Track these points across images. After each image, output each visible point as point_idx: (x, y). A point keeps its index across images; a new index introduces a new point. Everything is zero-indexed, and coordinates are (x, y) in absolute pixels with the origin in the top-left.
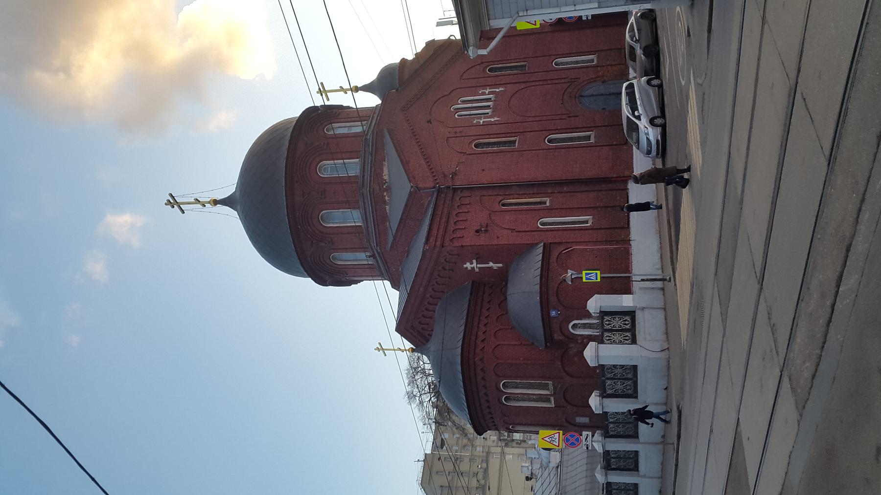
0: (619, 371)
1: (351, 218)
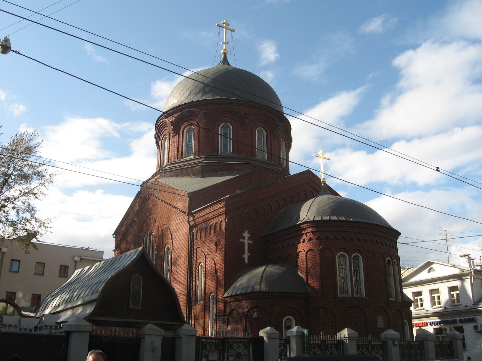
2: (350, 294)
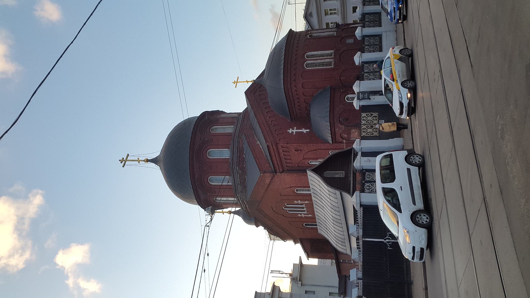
0: (372, 49)
1: (224, 154)
2: (331, 60)
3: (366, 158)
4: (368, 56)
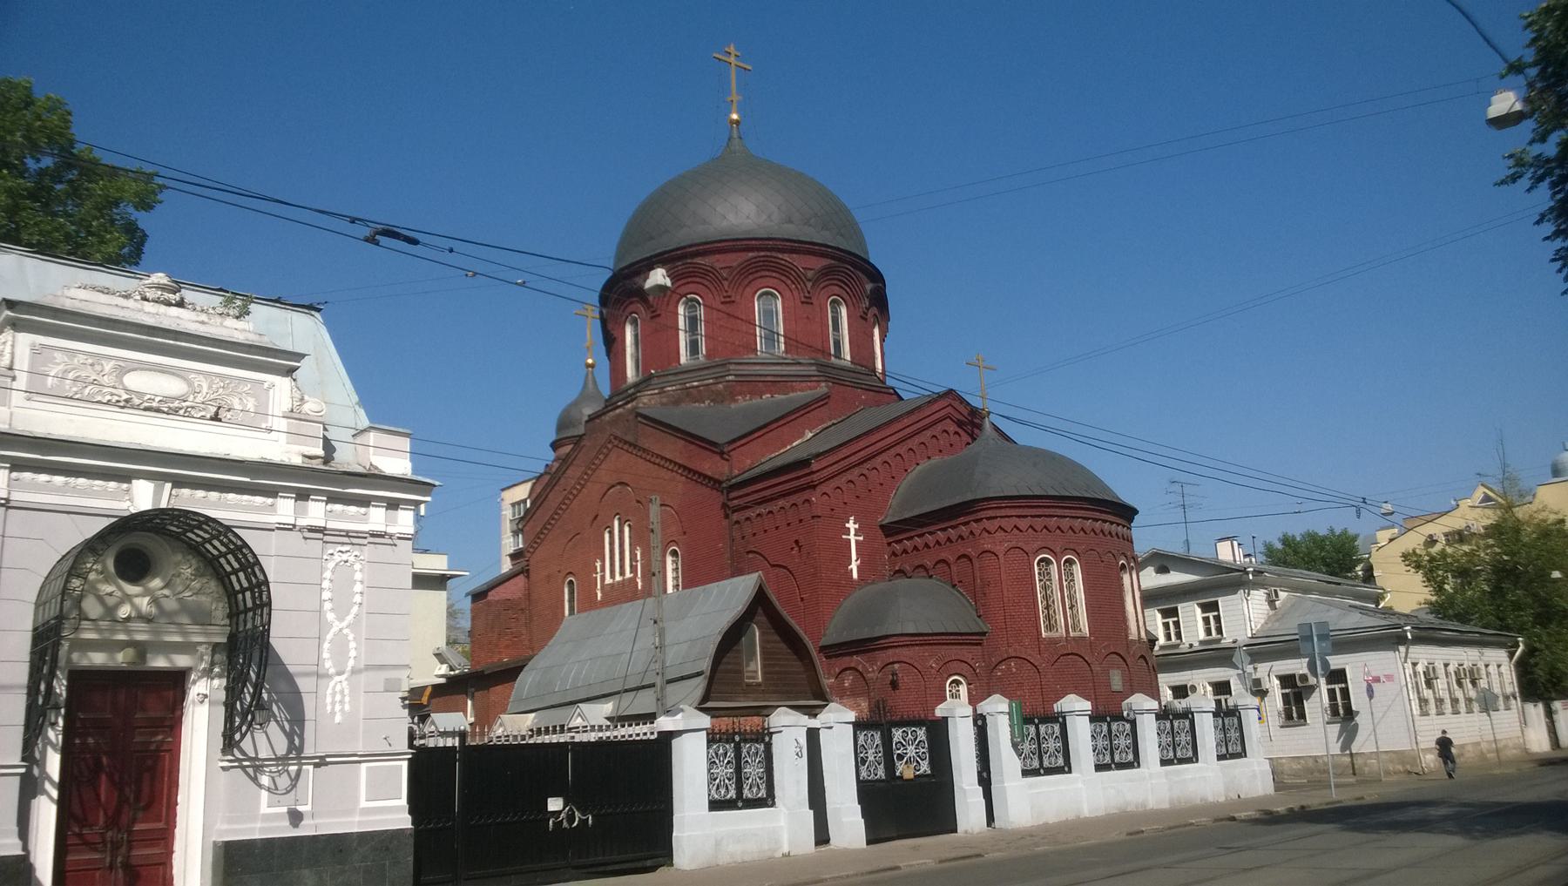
3: (803, 741)
4: (1081, 732)
